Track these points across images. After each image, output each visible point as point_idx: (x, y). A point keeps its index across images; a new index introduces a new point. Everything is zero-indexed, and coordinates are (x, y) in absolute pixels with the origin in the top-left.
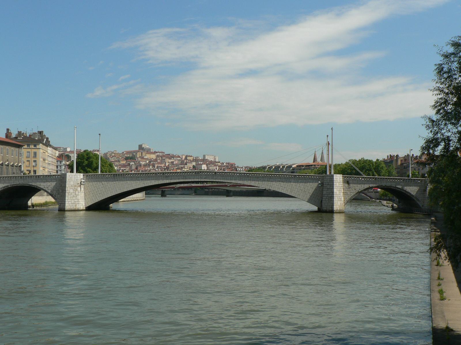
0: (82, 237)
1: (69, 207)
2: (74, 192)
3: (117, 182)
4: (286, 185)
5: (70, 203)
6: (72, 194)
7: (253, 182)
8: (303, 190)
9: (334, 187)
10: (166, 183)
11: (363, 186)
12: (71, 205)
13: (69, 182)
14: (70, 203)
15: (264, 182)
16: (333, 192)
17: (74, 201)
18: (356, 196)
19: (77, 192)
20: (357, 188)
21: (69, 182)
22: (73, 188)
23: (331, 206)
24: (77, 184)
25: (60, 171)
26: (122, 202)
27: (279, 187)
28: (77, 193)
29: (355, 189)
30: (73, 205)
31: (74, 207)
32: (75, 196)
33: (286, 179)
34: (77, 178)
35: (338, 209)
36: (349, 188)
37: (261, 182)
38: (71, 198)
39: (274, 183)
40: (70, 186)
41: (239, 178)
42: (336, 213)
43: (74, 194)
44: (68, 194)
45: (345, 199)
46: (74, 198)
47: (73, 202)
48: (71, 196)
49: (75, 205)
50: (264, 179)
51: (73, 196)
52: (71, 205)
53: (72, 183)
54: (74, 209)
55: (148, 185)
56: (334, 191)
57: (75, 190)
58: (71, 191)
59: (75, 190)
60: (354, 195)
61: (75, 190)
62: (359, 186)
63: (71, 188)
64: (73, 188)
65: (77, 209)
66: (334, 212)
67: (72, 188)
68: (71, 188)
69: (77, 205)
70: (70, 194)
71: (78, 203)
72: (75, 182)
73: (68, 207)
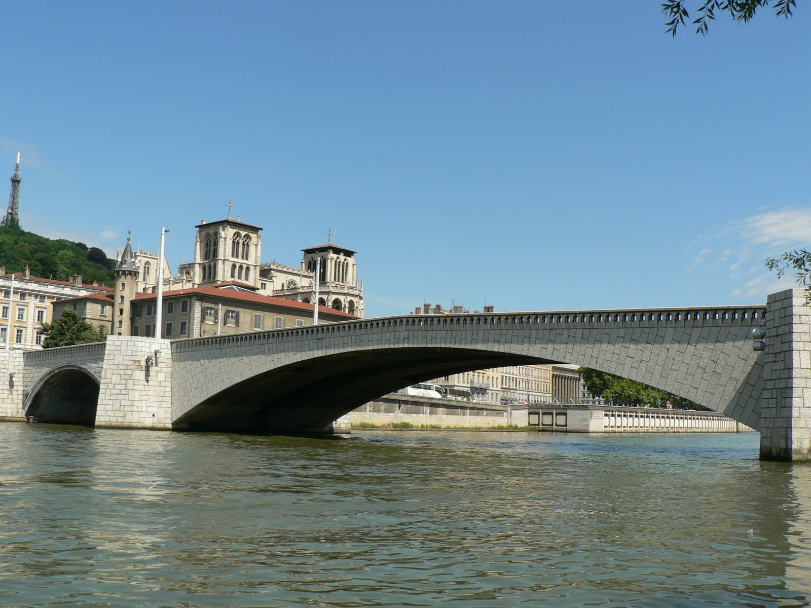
1: (107, 419)
2: (123, 382)
3: (225, 359)
4: (647, 352)
6: (117, 387)
7: (538, 347)
8: (710, 370)
9: (795, 345)
10: (318, 357)
12: (112, 413)
13: (112, 357)
15: (570, 346)
16: (790, 369)
17: (119, 404)
19: (130, 383)
21: (112, 357)
22: (122, 372)
23: (783, 432)
24: (132, 363)
26: (630, 433)
27: (622, 359)
28: (130, 386)
30: (116, 415)
31: (120, 420)
32: (123, 392)
33: (647, 330)
34: (133, 348)
38: (114, 397)
39: (604, 346)
40: (112, 367)
41: (497, 332)
43: (123, 387)
44: (105, 387)
46: (122, 397)
47: (116, 406)
48: (113, 392)
50: (572, 332)
51: (118, 392)
52: (112, 413)
53: (118, 360)
54: (120, 424)
55: (281, 365)
56: (792, 363)
58: (116, 379)
61: (124, 377)
64: (122, 372)
65: (126, 424)
66: (795, 457)
67: (118, 372)
69: (128, 415)
70: (111, 386)
71: (130, 408)
73: (102, 419)
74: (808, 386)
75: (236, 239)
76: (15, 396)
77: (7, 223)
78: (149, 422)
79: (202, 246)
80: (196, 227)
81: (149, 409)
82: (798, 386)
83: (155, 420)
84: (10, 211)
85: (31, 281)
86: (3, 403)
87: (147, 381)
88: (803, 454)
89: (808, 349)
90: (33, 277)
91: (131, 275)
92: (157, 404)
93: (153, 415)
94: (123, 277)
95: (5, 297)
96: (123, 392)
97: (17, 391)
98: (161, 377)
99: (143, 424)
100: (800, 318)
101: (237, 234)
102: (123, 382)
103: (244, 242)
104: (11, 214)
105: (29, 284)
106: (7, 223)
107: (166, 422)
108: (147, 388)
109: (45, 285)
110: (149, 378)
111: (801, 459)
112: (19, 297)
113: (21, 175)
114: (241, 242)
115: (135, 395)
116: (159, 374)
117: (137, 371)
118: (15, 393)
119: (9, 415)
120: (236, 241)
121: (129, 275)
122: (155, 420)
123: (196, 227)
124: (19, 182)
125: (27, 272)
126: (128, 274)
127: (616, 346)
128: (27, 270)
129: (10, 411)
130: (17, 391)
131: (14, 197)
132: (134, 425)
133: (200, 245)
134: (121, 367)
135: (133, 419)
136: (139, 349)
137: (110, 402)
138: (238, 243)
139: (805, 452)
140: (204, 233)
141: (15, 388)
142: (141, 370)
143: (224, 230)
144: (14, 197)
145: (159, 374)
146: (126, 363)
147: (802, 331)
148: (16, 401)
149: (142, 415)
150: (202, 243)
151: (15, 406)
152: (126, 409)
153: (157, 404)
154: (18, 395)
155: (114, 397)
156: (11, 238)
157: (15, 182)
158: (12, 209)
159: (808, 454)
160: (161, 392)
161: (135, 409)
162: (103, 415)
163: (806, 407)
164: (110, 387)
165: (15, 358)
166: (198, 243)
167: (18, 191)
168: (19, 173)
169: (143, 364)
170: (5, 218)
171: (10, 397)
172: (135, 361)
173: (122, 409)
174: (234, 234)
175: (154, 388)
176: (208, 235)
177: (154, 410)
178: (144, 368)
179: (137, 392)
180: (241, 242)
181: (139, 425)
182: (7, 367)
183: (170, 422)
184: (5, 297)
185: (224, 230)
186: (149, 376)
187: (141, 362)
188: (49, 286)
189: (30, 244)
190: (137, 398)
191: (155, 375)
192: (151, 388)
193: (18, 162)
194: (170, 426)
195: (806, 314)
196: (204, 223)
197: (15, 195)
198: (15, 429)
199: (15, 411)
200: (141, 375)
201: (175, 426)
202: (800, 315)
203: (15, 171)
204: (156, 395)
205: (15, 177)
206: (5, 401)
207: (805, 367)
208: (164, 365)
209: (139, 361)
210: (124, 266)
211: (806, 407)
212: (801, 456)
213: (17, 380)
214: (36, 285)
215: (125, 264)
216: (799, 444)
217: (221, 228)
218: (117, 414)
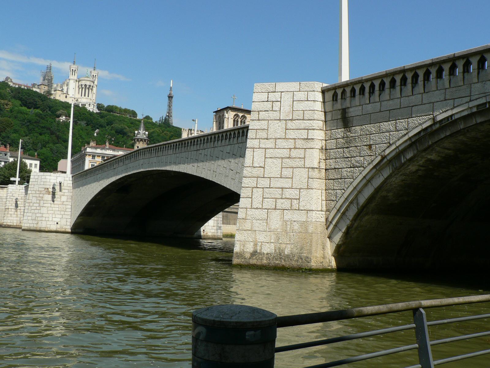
0: (320, 328)
1: (28, 225)
2: (38, 201)
5: (29, 218)
6: (35, 205)
11: (402, 123)
13: (33, 186)
14: (29, 218)
17: (35, 216)
18: (378, 182)
19: (42, 202)
20: (376, 138)
22: (38, 195)
25: (234, 187)
28: (41, 205)
29: (370, 146)
31: (35, 226)
32: (38, 208)
34: (45, 180)
35: (268, 249)
36: (348, 143)
37: (201, 164)
38: (33, 211)
40: (33, 192)
42: (241, 267)
43: (37, 205)
44: (28, 205)
45: (333, 203)
48: (33, 208)
49: (36, 222)
51: (35, 208)
53: (36, 188)
54: (35, 228)
57: (40, 198)
59: (40, 198)
60: (368, 181)
62: (385, 126)
63: (34, 195)
64: (38, 195)
65: (38, 229)
66: (235, 261)
67: (36, 195)
68: (34, 195)
69: (40, 223)
70: (31, 204)
71: (41, 219)
72: (41, 186)
74: (258, 186)
75: (236, 118)
76: (19, 213)
77: (162, 121)
78: (54, 228)
79: (217, 124)
80: (214, 112)
81: (54, 219)
82: (247, 186)
83: (58, 226)
84: (167, 114)
85: (109, 149)
86: (11, 217)
87: (53, 201)
88: (245, 258)
89: (264, 147)
90: (112, 146)
91: (142, 141)
92: (60, 216)
93: (57, 223)
94: (138, 143)
95: (92, 159)
96: (38, 208)
97: (20, 209)
98: (64, 199)
99: (49, 229)
100: (259, 114)
101: (237, 116)
102: (38, 201)
103: (234, 119)
104: (168, 116)
105: (107, 151)
106: (162, 121)
107: (67, 228)
108: (53, 206)
109: (117, 151)
110: (55, 199)
111: (241, 263)
112: (91, 157)
113: (173, 93)
114: (239, 120)
115: (44, 210)
116: (62, 197)
117: (46, 195)
118: (19, 211)
119: (15, 224)
120: (243, 121)
121: (141, 142)
122: (58, 226)
123: (214, 112)
124: (172, 97)
125: (107, 144)
126: (140, 141)
127: (225, 161)
128: (107, 143)
129: (15, 222)
130: (20, 209)
131: (170, 106)
132: (42, 229)
133: (216, 124)
134: (37, 192)
135: (43, 225)
136: (48, 180)
137: (30, 214)
138: (238, 121)
139: (248, 256)
140: (218, 116)
141: (19, 208)
142: (49, 194)
143: (227, 113)
144: (170, 106)
145: (62, 197)
146: (40, 189)
147: (259, 128)
148: (19, 216)
149: (48, 223)
150: (217, 122)
151: (19, 219)
152: (39, 219)
153: (60, 216)
154: (21, 212)
155: (33, 211)
156: (160, 129)
157: (170, 97)
158: (169, 113)
159: (250, 258)
160: (64, 208)
161: (44, 219)
162: (26, 222)
163: (254, 208)
164: (31, 205)
165: (20, 190)
166: (215, 123)
167: (172, 103)
168: (172, 92)
169: (51, 190)
170: (161, 118)
171: (16, 213)
172: (45, 189)
173: (36, 219)
174: (235, 115)
175: (58, 205)
176: (220, 116)
177: (58, 220)
178: (51, 193)
179: (45, 208)
180: (239, 120)
181: (46, 230)
182: (14, 195)
183: (70, 228)
184: (92, 159)
185: (227, 113)
186: (55, 198)
187: (49, 189)
188: (119, 152)
189: (171, 132)
190: (45, 211)
191: (59, 197)
192: (56, 206)
193: (171, 86)
194: (70, 230)
195: (266, 109)
196: (219, 109)
197: (170, 105)
198: (68, 236)
199: (19, 222)
200: (50, 197)
201: (73, 231)
202: (258, 111)
203: (170, 91)
204: (59, 210)
205: (170, 94)
206: (13, 215)
207: (258, 166)
208: (67, 191)
209: (48, 189)
210: (138, 136)
211: (254, 208)
212: (243, 260)
213: (20, 203)
214: (112, 151)
215: (139, 134)
216: (242, 248)
217: (225, 112)
218: (34, 222)
